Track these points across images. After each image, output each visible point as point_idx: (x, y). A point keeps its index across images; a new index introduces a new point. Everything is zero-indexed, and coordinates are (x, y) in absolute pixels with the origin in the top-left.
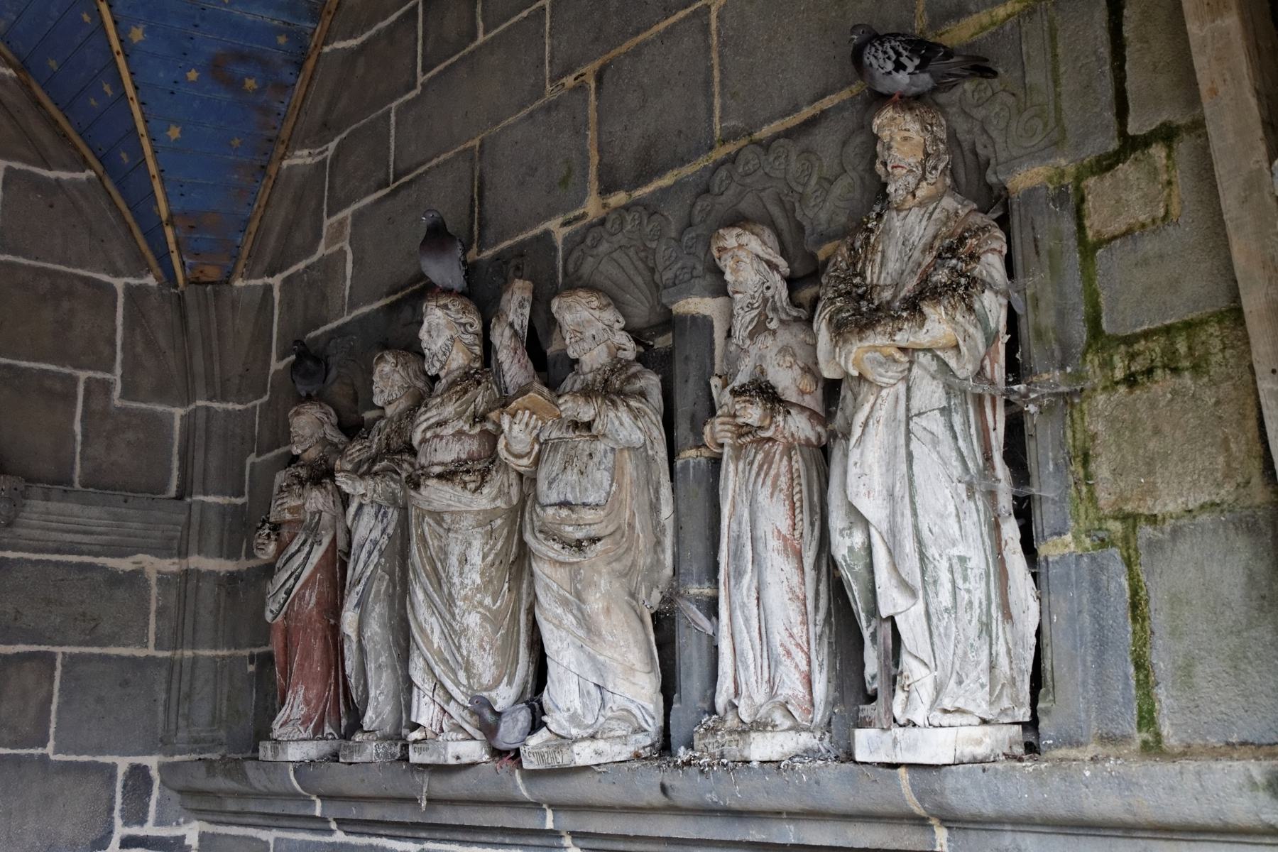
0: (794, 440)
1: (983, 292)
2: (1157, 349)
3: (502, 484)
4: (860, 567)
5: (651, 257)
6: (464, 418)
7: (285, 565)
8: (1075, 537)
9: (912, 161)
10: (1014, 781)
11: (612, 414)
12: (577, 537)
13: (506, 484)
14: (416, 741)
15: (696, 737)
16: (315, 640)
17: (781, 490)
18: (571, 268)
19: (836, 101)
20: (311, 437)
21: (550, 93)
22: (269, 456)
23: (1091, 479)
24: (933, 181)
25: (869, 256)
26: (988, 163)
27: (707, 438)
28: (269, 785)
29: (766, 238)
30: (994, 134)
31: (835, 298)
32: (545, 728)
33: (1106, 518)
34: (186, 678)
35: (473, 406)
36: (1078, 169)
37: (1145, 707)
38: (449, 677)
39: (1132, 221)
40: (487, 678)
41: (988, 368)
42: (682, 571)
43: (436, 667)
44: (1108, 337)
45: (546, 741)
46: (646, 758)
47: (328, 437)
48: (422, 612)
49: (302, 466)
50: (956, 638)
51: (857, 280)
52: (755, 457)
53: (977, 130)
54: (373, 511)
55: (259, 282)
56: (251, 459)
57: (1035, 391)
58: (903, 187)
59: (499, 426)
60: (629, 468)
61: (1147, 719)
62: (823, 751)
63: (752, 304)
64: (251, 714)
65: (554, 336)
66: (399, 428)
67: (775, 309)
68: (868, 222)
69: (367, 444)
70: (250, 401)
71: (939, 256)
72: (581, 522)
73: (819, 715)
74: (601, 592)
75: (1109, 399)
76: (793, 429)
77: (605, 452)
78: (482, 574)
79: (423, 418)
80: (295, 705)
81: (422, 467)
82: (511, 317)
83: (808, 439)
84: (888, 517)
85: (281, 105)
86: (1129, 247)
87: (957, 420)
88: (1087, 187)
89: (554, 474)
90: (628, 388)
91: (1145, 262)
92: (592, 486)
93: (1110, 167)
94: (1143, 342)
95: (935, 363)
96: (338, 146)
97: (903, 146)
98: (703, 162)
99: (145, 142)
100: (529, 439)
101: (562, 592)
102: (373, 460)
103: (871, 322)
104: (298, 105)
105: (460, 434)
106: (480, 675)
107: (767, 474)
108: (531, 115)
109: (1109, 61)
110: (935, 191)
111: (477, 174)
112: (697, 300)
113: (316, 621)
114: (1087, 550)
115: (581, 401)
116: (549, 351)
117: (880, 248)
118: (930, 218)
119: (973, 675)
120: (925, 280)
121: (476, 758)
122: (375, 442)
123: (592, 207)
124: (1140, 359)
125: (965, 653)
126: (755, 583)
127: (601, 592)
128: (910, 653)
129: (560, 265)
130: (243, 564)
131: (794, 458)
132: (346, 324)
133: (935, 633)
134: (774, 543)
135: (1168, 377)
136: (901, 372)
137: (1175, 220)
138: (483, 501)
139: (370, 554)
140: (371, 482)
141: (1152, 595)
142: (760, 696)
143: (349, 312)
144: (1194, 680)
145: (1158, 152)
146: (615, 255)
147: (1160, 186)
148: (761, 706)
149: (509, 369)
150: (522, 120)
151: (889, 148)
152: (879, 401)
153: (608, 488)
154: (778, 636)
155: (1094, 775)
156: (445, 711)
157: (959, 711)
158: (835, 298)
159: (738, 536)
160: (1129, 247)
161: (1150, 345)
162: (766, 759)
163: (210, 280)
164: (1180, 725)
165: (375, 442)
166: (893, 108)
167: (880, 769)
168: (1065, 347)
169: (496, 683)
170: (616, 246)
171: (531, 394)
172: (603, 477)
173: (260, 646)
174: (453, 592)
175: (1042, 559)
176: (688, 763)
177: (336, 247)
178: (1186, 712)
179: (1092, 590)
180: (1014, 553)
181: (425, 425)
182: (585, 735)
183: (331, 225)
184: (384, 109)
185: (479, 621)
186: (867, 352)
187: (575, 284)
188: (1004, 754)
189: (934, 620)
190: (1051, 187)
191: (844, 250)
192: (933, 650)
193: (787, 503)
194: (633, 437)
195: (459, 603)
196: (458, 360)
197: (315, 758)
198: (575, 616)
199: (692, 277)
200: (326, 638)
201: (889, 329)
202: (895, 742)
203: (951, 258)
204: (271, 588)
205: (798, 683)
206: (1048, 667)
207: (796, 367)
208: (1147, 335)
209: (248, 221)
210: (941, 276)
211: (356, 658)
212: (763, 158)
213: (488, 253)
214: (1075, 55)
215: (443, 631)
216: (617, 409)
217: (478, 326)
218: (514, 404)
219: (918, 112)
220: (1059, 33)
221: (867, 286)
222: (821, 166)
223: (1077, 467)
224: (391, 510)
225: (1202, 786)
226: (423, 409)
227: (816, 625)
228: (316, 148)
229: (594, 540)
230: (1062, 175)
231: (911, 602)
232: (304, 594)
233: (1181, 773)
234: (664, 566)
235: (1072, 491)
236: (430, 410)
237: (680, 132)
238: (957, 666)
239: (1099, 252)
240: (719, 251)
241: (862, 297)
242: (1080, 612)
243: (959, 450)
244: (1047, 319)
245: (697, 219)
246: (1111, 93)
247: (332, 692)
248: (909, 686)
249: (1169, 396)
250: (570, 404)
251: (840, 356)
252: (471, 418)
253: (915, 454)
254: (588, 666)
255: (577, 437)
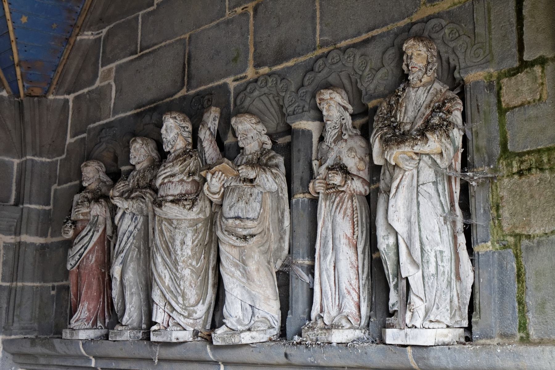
0: (354, 192)
1: (454, 129)
2: (534, 159)
3: (202, 206)
4: (392, 254)
5: (281, 100)
6: (184, 173)
7: (79, 241)
8: (492, 244)
9: (421, 65)
10: (464, 354)
11: (264, 176)
12: (244, 234)
13: (204, 207)
14: (155, 331)
15: (303, 331)
16: (94, 279)
17: (348, 216)
18: (238, 102)
19: (380, 32)
20: (93, 177)
21: (228, 15)
22: (65, 186)
23: (500, 217)
24: (430, 75)
25: (399, 108)
26: (455, 68)
27: (311, 190)
28: (67, 351)
29: (343, 95)
30: (459, 54)
31: (383, 127)
32: (224, 325)
33: (506, 235)
34: (18, 296)
35: (188, 168)
36: (499, 74)
37: (522, 322)
38: (173, 300)
39: (524, 100)
40: (192, 301)
41: (454, 164)
42: (294, 252)
43: (167, 295)
44: (510, 153)
45: (225, 332)
46: (274, 341)
47: (101, 178)
48: (160, 268)
49: (89, 192)
50: (436, 288)
51: (393, 119)
52: (335, 199)
53: (450, 51)
54: (130, 217)
55: (62, 97)
56: (54, 187)
57: (476, 176)
58: (416, 77)
59: (205, 180)
60: (269, 201)
61: (523, 327)
62: (366, 339)
63: (335, 127)
64: (53, 315)
65: (229, 135)
66: (144, 175)
67: (346, 129)
68: (398, 92)
69: (127, 183)
70: (54, 157)
71: (433, 111)
72: (246, 227)
73: (364, 322)
74: (255, 261)
75: (510, 181)
76: (355, 187)
77: (258, 193)
78: (192, 250)
79: (163, 172)
80: (83, 312)
81: (162, 197)
82: (209, 125)
83: (361, 192)
84: (408, 231)
85: (78, 8)
86: (522, 112)
87: (440, 187)
88: (503, 83)
89: (232, 203)
90: (270, 163)
91: (529, 119)
92: (252, 210)
93: (514, 75)
94: (527, 156)
95: (430, 160)
96: (108, 31)
97: (418, 58)
98: (311, 55)
99: (10, 24)
100: (220, 185)
101: (235, 260)
102: (131, 191)
103: (403, 140)
104: (87, 9)
105: (182, 181)
106: (189, 299)
107: (341, 208)
108: (218, 25)
109: (515, 25)
110: (430, 80)
111: (187, 51)
112: (305, 122)
113: (94, 270)
114: (497, 249)
115: (250, 168)
116: (225, 143)
117: (404, 105)
118: (428, 92)
119: (443, 305)
120: (427, 121)
121: (186, 339)
122: (131, 182)
123: (250, 73)
124: (525, 164)
125: (441, 295)
126: (333, 259)
127: (255, 261)
128: (414, 294)
129: (232, 100)
130: (50, 240)
131: (354, 201)
132: (112, 122)
133: (426, 285)
134: (344, 241)
135: (538, 172)
136: (416, 164)
137: (544, 101)
138: (193, 215)
139: (128, 238)
140: (131, 203)
141: (527, 271)
142: (334, 312)
143: (113, 116)
144: (546, 310)
145: (538, 69)
146: (262, 98)
147: (538, 85)
148: (335, 317)
149: (208, 151)
150: (213, 27)
151: (411, 58)
152: (404, 177)
153: (259, 211)
154: (344, 285)
155: (502, 352)
156: (170, 316)
157: (438, 321)
158: (383, 127)
159: (326, 236)
160: (522, 112)
161: (530, 157)
162: (340, 342)
163: (36, 95)
164: (538, 330)
165: (131, 182)
166: (414, 40)
167: (398, 348)
168: (491, 156)
169: (197, 303)
170: (263, 93)
171: (224, 164)
172: (257, 205)
173: (58, 282)
174: (177, 258)
175: (476, 253)
176: (300, 343)
177: (106, 83)
178: (541, 324)
179: (499, 268)
180: (463, 250)
181: (164, 176)
182: (244, 329)
183: (103, 71)
184: (135, 15)
185: (190, 273)
186: (400, 154)
187: (240, 111)
188: (457, 342)
189: (426, 279)
190: (486, 81)
191: (385, 104)
192: (425, 293)
193: (350, 222)
194: (273, 187)
195: (180, 264)
196: (180, 144)
197: (93, 338)
198: (240, 272)
199: (303, 111)
200: (99, 278)
201: (411, 144)
202: (406, 335)
203: (439, 112)
204: (71, 253)
205: (353, 306)
206: (477, 302)
207: (356, 158)
208: (529, 153)
209: (57, 66)
210: (435, 120)
211: (118, 290)
212: (342, 56)
213: (192, 92)
214: (499, 21)
215: (171, 277)
216: (266, 173)
217: (190, 128)
218: (214, 168)
219: (425, 43)
220: (492, 10)
221: (398, 122)
222: (371, 63)
223: (493, 212)
224: (139, 216)
225: (552, 357)
226: (163, 168)
227: (362, 280)
228: (95, 31)
229: (252, 236)
230: (491, 76)
231: (416, 270)
232: (89, 256)
233: (543, 351)
234: (284, 249)
235: (491, 222)
236: (167, 168)
237: (298, 40)
238: (437, 301)
239: (508, 113)
240: (320, 100)
241: (395, 127)
242: (493, 278)
243: (441, 201)
244: (482, 143)
245: (306, 83)
246: (516, 40)
247: (101, 306)
248: (413, 309)
249: (538, 181)
250: (244, 170)
251: (387, 155)
252: (187, 174)
253: (421, 203)
254: (246, 296)
255: (245, 186)
